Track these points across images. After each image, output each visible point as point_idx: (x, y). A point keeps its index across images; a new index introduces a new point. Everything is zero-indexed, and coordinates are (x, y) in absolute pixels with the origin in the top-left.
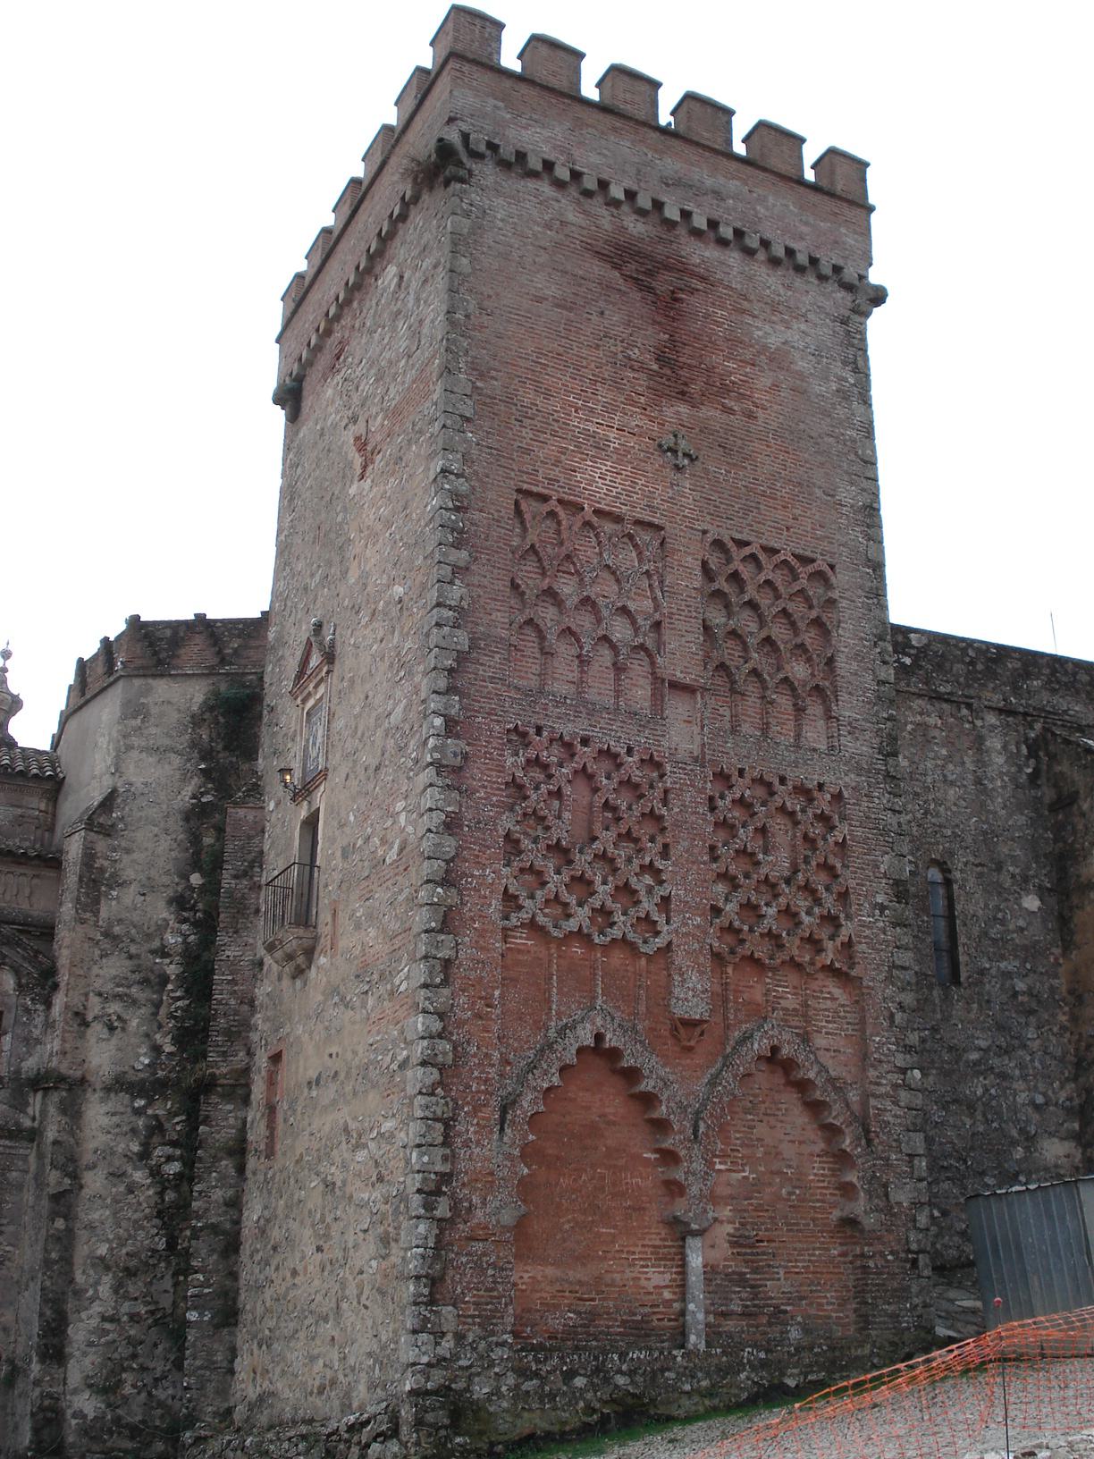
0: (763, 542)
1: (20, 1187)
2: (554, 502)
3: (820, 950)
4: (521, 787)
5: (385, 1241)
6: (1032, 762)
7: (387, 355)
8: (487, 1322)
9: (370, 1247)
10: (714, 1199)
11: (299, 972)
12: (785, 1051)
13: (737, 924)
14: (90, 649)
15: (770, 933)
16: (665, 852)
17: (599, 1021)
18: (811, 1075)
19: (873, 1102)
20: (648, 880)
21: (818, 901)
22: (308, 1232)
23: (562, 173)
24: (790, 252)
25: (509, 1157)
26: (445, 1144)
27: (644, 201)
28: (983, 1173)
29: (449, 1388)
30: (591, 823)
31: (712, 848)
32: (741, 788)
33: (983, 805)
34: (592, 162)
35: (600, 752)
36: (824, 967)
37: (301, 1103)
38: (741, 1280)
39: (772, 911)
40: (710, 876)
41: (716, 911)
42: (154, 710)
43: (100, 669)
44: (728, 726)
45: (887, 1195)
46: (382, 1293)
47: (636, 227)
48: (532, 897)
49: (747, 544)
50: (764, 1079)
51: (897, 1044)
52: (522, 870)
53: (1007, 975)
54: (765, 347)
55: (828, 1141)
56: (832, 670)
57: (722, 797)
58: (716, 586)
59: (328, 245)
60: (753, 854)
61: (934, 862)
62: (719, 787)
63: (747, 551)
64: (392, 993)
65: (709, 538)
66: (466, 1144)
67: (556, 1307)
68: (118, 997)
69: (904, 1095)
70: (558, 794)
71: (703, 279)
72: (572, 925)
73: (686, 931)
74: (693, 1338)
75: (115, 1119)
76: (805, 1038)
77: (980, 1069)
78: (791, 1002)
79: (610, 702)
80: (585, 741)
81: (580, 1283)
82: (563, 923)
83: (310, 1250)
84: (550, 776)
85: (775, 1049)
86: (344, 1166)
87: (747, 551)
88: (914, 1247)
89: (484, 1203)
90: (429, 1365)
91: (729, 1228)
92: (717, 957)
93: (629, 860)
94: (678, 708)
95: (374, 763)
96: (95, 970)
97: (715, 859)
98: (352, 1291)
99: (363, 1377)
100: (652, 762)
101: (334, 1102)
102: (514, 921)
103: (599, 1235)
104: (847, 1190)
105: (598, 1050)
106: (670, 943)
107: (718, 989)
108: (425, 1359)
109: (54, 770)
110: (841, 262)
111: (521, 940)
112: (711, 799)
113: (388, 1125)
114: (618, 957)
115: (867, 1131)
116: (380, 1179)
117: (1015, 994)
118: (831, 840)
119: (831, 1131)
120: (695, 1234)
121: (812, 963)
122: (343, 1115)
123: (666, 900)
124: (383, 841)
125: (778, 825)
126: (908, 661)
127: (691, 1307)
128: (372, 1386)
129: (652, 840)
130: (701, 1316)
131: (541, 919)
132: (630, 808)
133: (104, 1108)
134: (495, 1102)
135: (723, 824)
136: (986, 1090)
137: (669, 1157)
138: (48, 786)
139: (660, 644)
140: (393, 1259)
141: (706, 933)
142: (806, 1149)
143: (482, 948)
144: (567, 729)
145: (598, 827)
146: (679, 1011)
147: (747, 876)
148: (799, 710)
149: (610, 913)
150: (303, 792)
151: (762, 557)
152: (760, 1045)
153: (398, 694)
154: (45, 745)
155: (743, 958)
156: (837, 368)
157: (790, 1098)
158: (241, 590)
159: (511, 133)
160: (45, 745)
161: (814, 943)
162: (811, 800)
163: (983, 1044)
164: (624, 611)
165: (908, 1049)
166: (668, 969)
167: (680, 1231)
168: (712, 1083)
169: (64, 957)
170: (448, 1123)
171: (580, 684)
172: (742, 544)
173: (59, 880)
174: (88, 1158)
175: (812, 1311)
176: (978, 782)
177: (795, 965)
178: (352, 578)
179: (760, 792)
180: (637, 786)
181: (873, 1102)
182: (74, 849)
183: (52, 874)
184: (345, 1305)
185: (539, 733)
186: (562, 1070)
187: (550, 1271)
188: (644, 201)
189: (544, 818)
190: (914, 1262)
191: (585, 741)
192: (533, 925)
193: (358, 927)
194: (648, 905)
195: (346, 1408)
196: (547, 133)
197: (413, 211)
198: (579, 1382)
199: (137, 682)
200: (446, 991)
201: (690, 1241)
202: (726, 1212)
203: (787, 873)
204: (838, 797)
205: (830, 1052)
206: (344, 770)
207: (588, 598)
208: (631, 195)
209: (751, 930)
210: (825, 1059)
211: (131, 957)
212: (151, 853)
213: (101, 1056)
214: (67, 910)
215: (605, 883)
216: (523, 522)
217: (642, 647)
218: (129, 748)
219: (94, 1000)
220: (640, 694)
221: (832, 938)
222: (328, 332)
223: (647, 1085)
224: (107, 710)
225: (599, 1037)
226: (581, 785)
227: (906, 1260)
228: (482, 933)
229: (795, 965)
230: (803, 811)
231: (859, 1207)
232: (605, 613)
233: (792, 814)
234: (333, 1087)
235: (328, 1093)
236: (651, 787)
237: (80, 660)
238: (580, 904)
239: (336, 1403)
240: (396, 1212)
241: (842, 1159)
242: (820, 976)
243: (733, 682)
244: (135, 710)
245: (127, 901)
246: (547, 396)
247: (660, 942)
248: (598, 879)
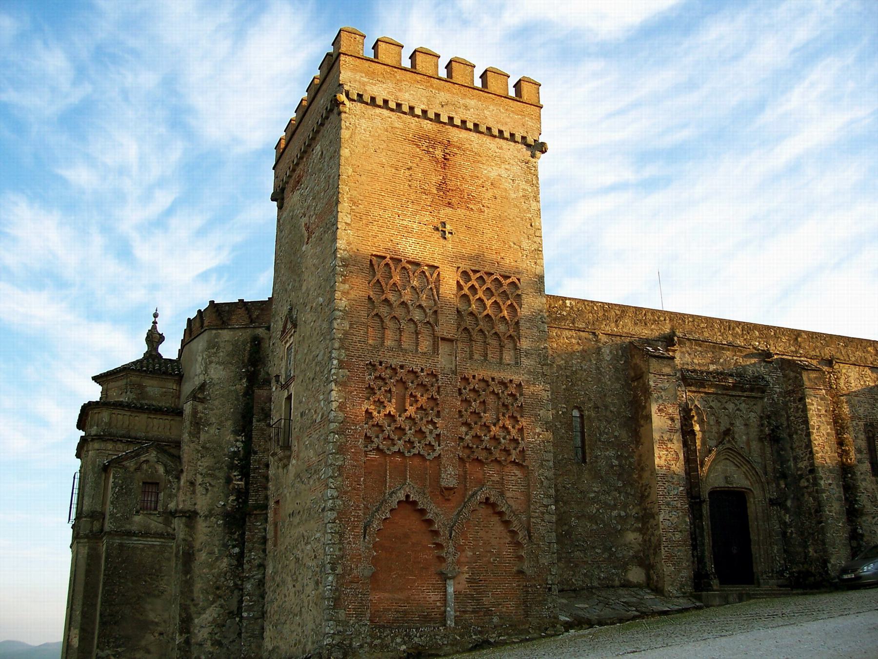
0: (486, 270)
1: (169, 559)
2: (387, 259)
3: (509, 454)
4: (373, 389)
5: (317, 583)
6: (624, 358)
7: (317, 188)
8: (359, 616)
9: (312, 585)
10: (459, 563)
11: (285, 466)
12: (492, 500)
13: (470, 445)
14: (193, 315)
15: (486, 448)
16: (438, 415)
17: (407, 490)
18: (504, 509)
19: (532, 520)
20: (430, 427)
21: (509, 433)
22: (290, 579)
23: (392, 105)
24: (501, 132)
25: (367, 548)
26: (339, 543)
27: (431, 115)
28: (594, 548)
29: (342, 643)
30: (404, 403)
31: (460, 412)
32: (474, 384)
33: (600, 380)
34: (407, 98)
35: (409, 371)
36: (511, 462)
37: (286, 524)
38: (472, 598)
39: (487, 438)
40: (459, 424)
41: (461, 439)
42: (222, 345)
43: (198, 325)
44: (468, 356)
45: (538, 560)
46: (316, 604)
47: (427, 125)
48: (377, 437)
49: (478, 271)
50: (483, 511)
51: (544, 494)
52: (373, 426)
53: (608, 458)
54: (488, 178)
55: (513, 537)
56: (518, 327)
57: (465, 389)
58: (463, 292)
59: (292, 130)
60: (479, 413)
61: (576, 407)
62: (464, 383)
63: (478, 275)
64: (319, 479)
65: (460, 270)
66: (349, 543)
67: (390, 610)
68: (211, 475)
69: (547, 517)
70: (390, 391)
71: (459, 148)
72: (396, 449)
73: (446, 449)
74: (449, 622)
75: (210, 529)
76: (502, 494)
77: (594, 501)
78: (496, 478)
79: (413, 347)
80: (402, 367)
81: (400, 600)
82: (391, 448)
83: (290, 586)
84: (386, 383)
85: (487, 499)
86: (303, 551)
87: (478, 275)
88: (550, 582)
89: (357, 567)
90: (334, 634)
91: (467, 576)
92: (461, 459)
93: (422, 419)
94: (444, 348)
95: (312, 376)
96: (199, 463)
97: (461, 416)
98: (306, 604)
99: (310, 640)
100: (433, 375)
101: (299, 524)
102: (370, 448)
103: (409, 579)
104: (520, 558)
105: (408, 502)
106: (440, 455)
107: (462, 473)
108: (332, 632)
109: (179, 371)
110: (525, 135)
111: (373, 455)
112: (460, 389)
113: (318, 535)
114: (417, 461)
115: (529, 533)
116: (315, 557)
117: (612, 466)
118: (515, 405)
119: (514, 533)
120: (450, 578)
121: (505, 460)
122: (301, 530)
123: (438, 435)
124: (315, 412)
125: (491, 399)
126: (565, 313)
127: (448, 609)
128: (313, 643)
129: (432, 409)
130: (452, 613)
131: (381, 447)
132: (422, 396)
133: (204, 525)
134: (362, 525)
135: (466, 401)
136: (598, 510)
137: (439, 546)
138: (176, 378)
139: (437, 322)
140: (320, 591)
141: (456, 449)
142: (502, 541)
143: (356, 461)
144: (394, 362)
145: (407, 405)
146: (443, 484)
147: (476, 423)
148: (502, 347)
149: (413, 443)
150: (286, 386)
151: (485, 277)
152: (480, 497)
153: (321, 347)
154: (175, 356)
155: (473, 459)
156: (523, 185)
157: (495, 519)
158: (259, 287)
159: (368, 88)
160: (175, 356)
161: (507, 452)
162: (506, 387)
163: (596, 489)
164: (420, 306)
165: (549, 497)
166: (439, 465)
167: (444, 577)
168: (458, 514)
169: (185, 458)
170: (341, 535)
171: (399, 341)
172: (475, 272)
173: (182, 422)
174: (197, 546)
175: (504, 610)
176: (598, 368)
177: (497, 461)
178: (304, 288)
179: (482, 385)
180: (425, 386)
181: (532, 520)
182: (188, 408)
183: (178, 419)
184: (303, 610)
185: (381, 365)
186: (391, 510)
187: (386, 595)
188: (431, 115)
189: (383, 402)
190: (550, 589)
191: (402, 367)
192: (378, 449)
193: (306, 449)
194: (430, 438)
195: (304, 652)
196: (384, 86)
197: (327, 122)
198: (398, 640)
199: (214, 332)
200: (340, 479)
201: (448, 581)
202: (466, 568)
203: (494, 421)
204: (519, 385)
205: (513, 499)
206: (301, 378)
207: (403, 302)
208: (424, 112)
209: (477, 447)
210: (511, 502)
211: (215, 457)
212: (220, 412)
213: (202, 503)
214: (186, 437)
215: (410, 429)
216: (374, 269)
217: (428, 322)
218: (211, 362)
219: (199, 476)
220: (425, 345)
221: (515, 449)
222: (294, 170)
223: (430, 516)
224: (200, 344)
225: (408, 496)
226: (400, 385)
227: (546, 588)
228: (355, 454)
229: (497, 461)
230: (503, 392)
231: (525, 566)
232: (411, 308)
233: (498, 394)
234: (298, 517)
235: (296, 520)
236: (432, 386)
237: (189, 319)
238: (399, 439)
239: (301, 650)
240: (321, 571)
241: (518, 544)
242: (510, 465)
243: (471, 336)
244: (213, 345)
245: (212, 431)
246: (385, 210)
247: (436, 454)
248: (407, 428)
